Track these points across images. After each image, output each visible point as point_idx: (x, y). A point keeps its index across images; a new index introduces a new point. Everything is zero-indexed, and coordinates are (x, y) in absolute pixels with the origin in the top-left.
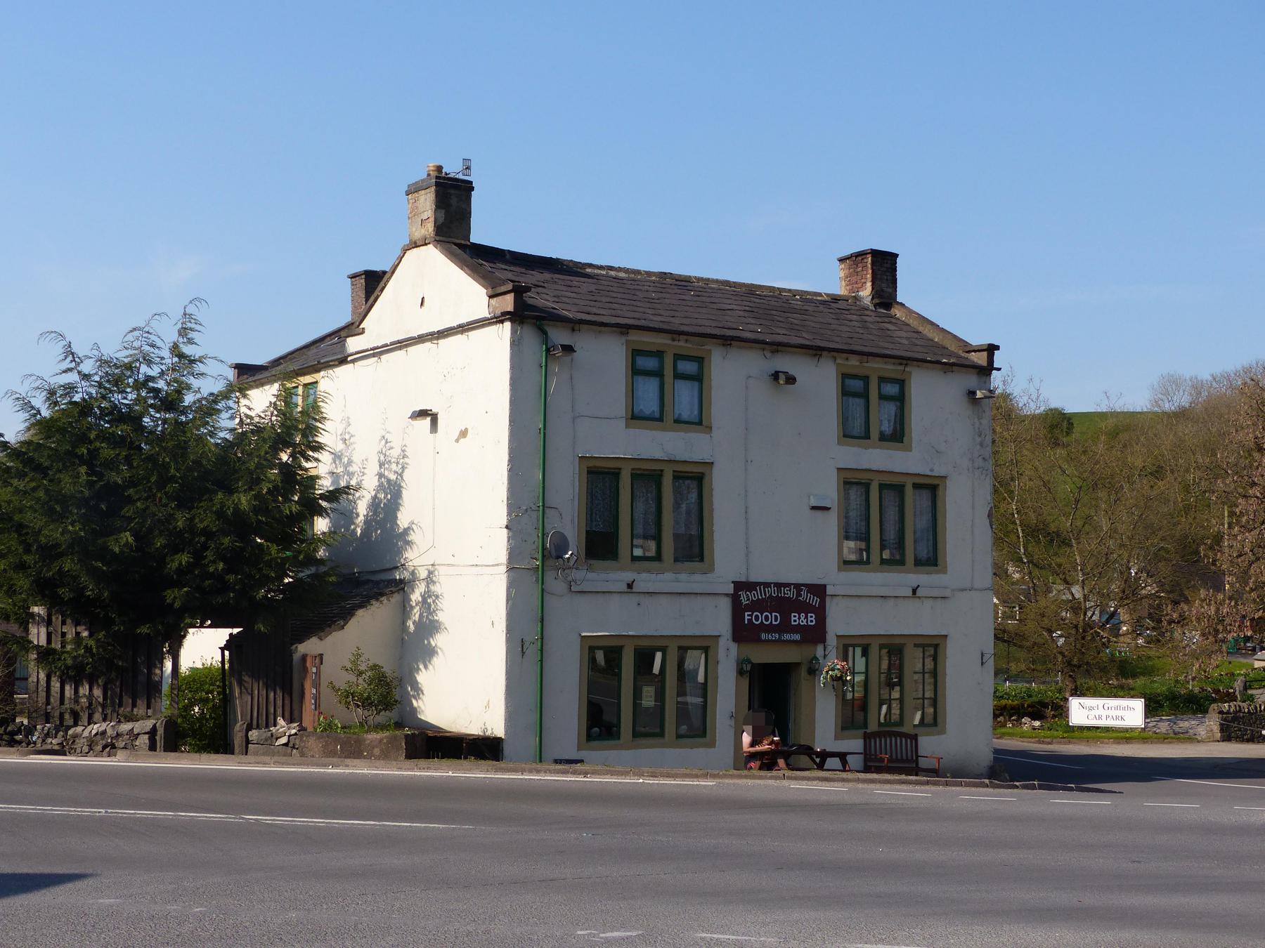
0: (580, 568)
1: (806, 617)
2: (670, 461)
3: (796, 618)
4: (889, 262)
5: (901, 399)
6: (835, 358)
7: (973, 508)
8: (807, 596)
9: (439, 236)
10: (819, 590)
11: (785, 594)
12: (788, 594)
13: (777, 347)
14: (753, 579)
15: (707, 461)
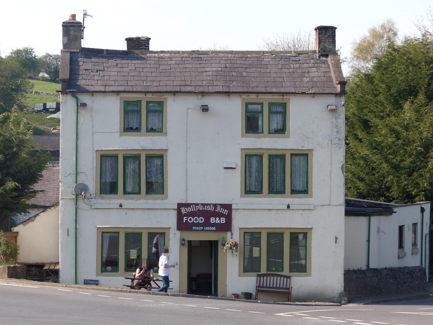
0: (97, 198)
1: (220, 219)
2: (143, 150)
3: (214, 220)
4: (330, 32)
5: (284, 114)
6: (241, 96)
7: (331, 164)
8: (220, 209)
9: (66, 49)
10: (228, 207)
11: (207, 208)
12: (209, 209)
13: (203, 94)
14: (189, 202)
15: (164, 149)
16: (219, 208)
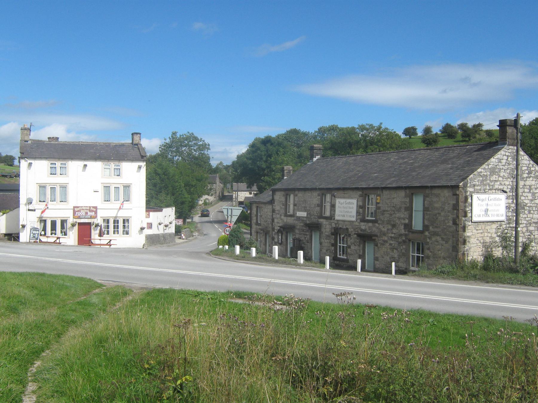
16: (91, 208)
